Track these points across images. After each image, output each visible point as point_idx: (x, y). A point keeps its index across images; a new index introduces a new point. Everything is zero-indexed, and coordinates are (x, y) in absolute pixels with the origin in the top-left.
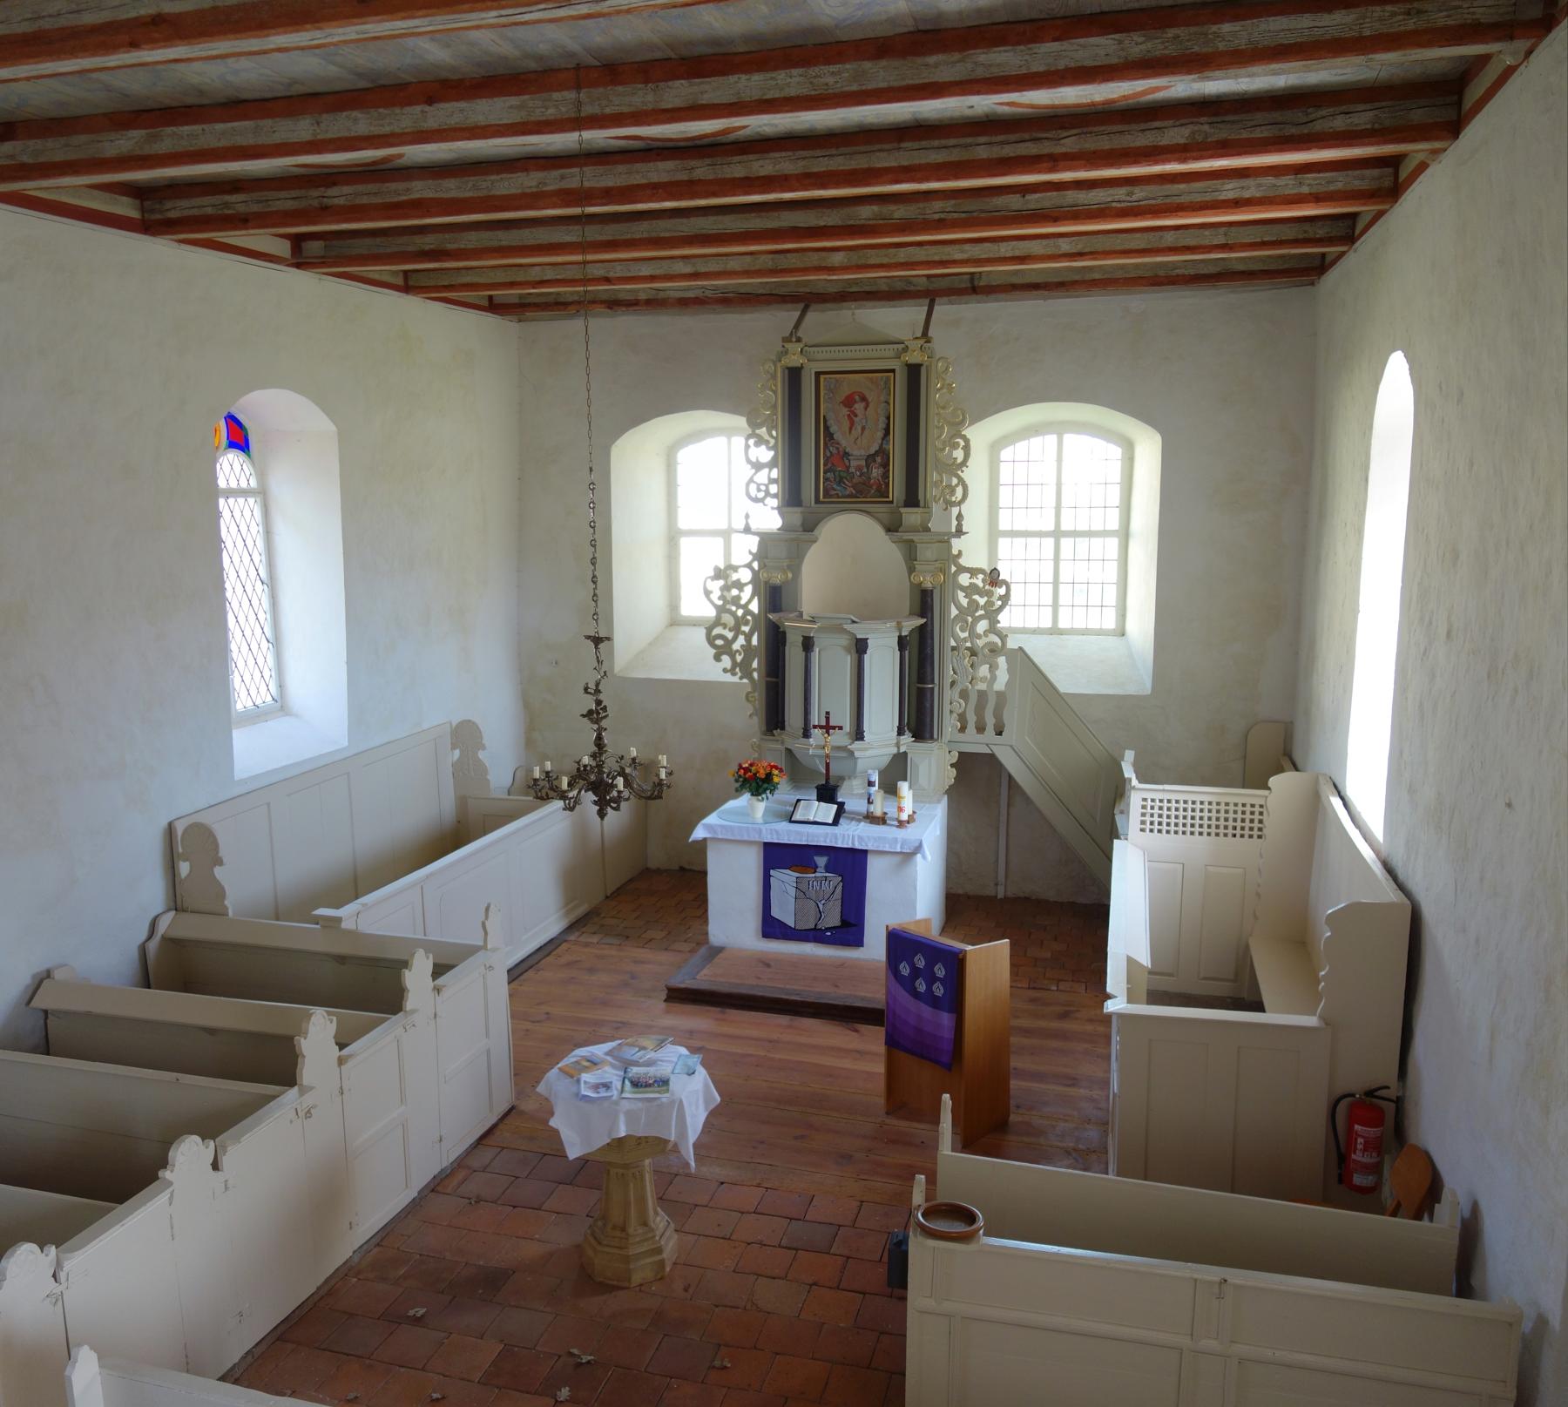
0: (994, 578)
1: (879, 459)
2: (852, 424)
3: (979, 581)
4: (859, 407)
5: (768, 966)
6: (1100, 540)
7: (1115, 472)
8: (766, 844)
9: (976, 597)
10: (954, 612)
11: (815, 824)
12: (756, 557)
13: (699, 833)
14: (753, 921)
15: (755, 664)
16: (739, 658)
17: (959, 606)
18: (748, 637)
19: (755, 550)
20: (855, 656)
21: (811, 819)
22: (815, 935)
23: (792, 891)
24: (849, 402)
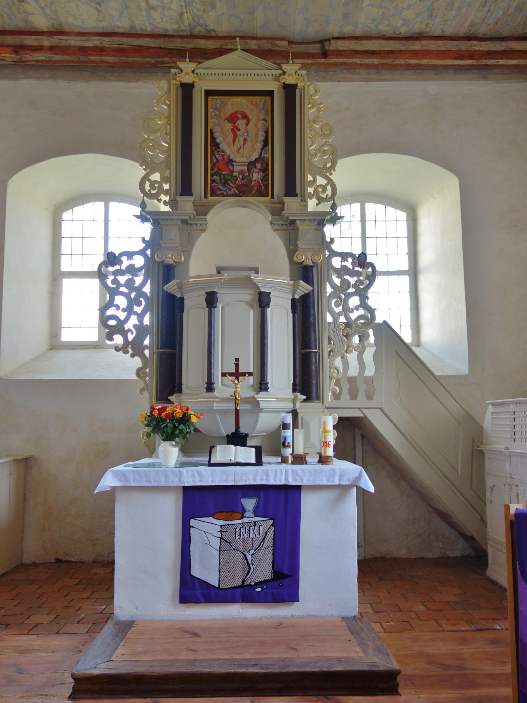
0: (361, 260)
1: (259, 166)
2: (235, 136)
3: (349, 263)
4: (241, 123)
5: (196, 635)
6: (401, 269)
7: (403, 229)
8: (186, 489)
9: (347, 277)
10: (329, 290)
11: (233, 467)
12: (148, 244)
13: (108, 481)
14: (169, 583)
15: (147, 342)
16: (130, 337)
17: (333, 285)
18: (141, 317)
19: (147, 238)
20: (258, 310)
21: (233, 460)
22: (244, 594)
23: (216, 543)
24: (232, 119)
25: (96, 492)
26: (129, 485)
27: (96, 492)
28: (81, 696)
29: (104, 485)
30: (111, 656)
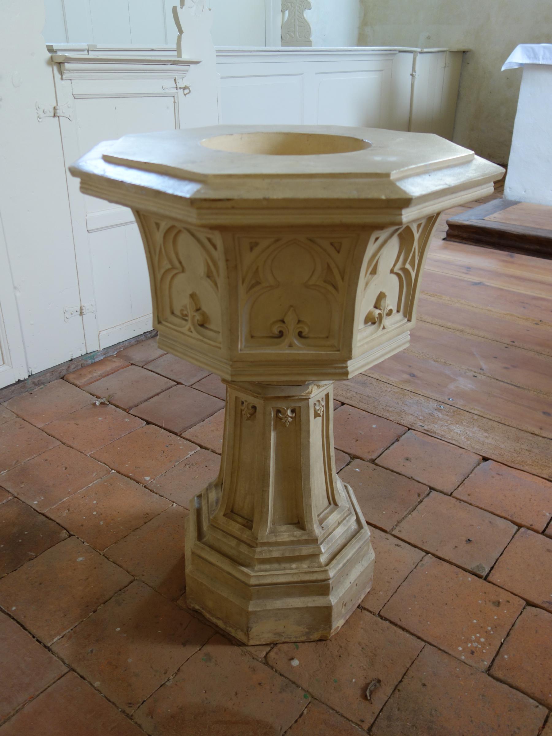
13: (518, 57)
25: (503, 69)
26: (537, 62)
27: (503, 69)
28: (453, 239)
29: (511, 61)
30: (485, 216)
